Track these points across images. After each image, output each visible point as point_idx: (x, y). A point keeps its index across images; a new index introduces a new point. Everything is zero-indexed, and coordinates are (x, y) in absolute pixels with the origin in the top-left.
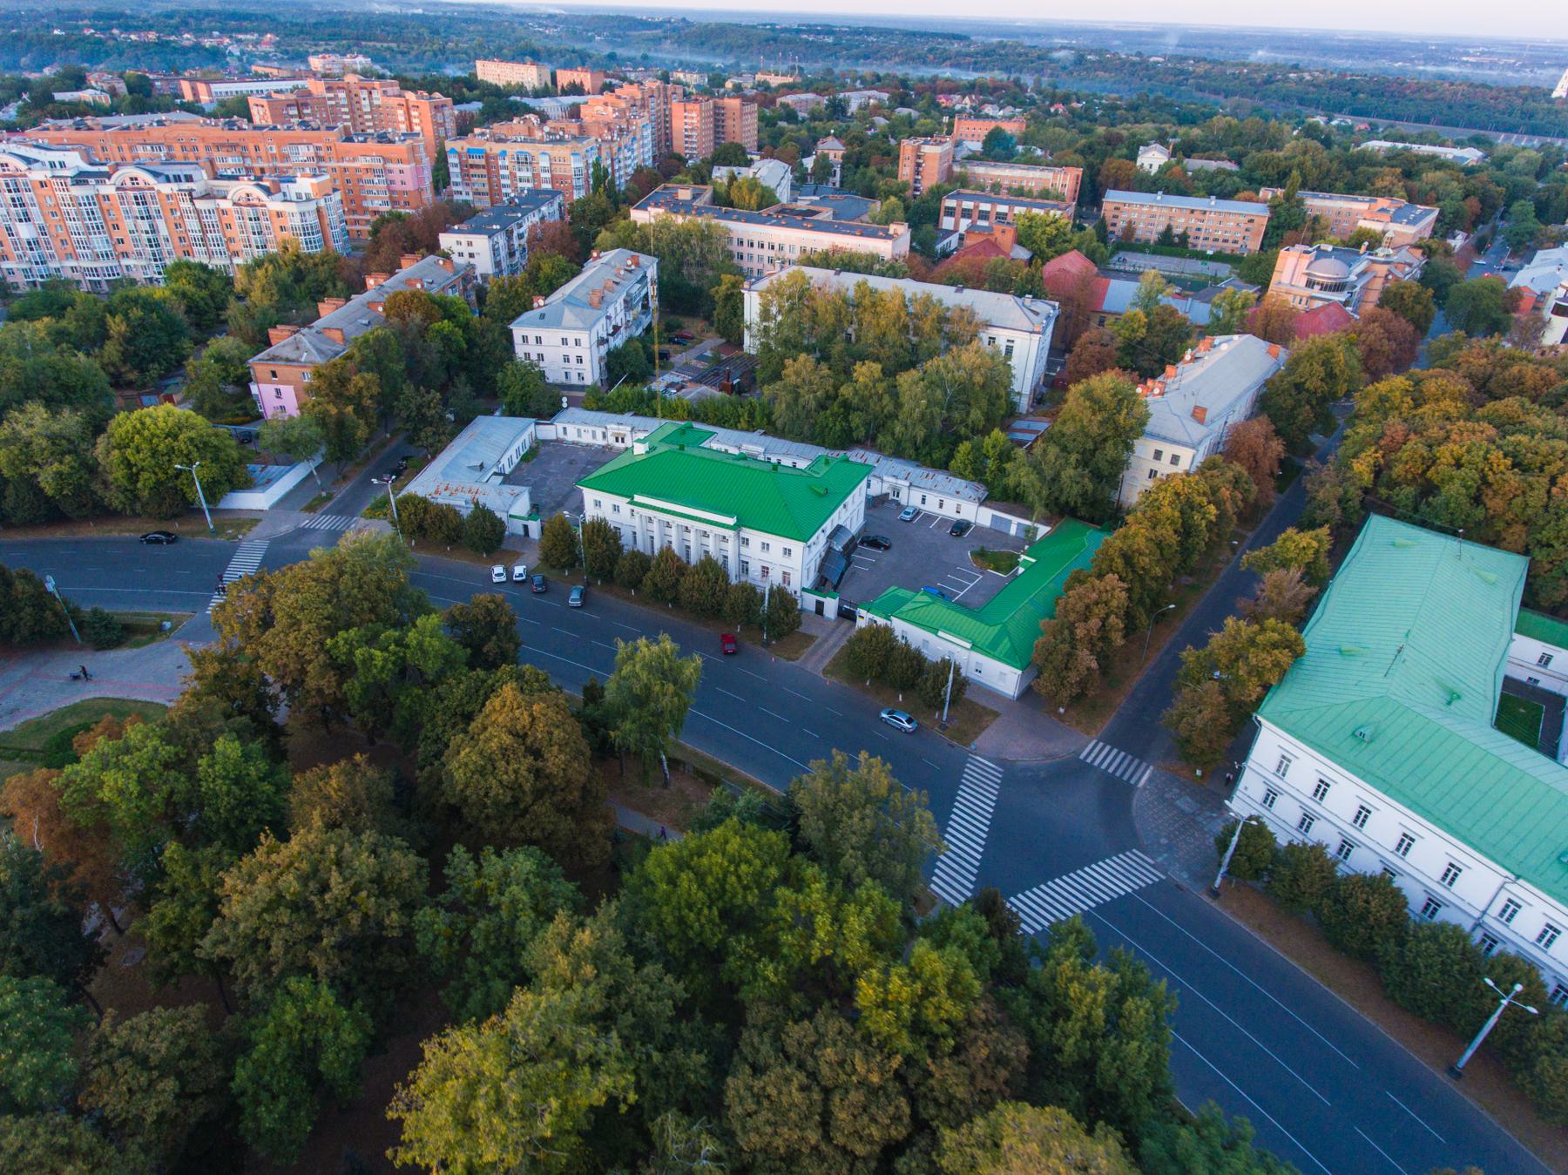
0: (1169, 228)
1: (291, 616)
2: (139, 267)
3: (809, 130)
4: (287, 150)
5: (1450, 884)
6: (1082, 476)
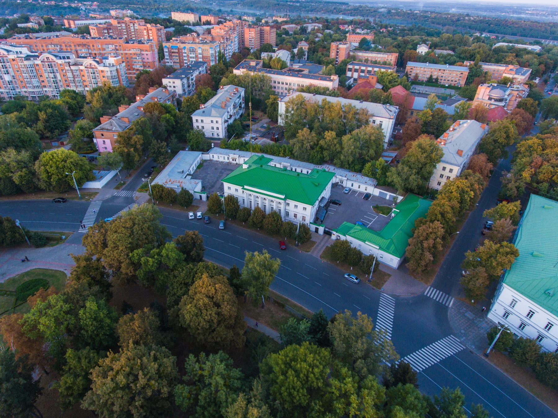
0: (431, 76)
1: (114, 243)
2: (50, 91)
3: (294, 38)
4: (104, 46)
5: (548, 330)
6: (418, 178)
